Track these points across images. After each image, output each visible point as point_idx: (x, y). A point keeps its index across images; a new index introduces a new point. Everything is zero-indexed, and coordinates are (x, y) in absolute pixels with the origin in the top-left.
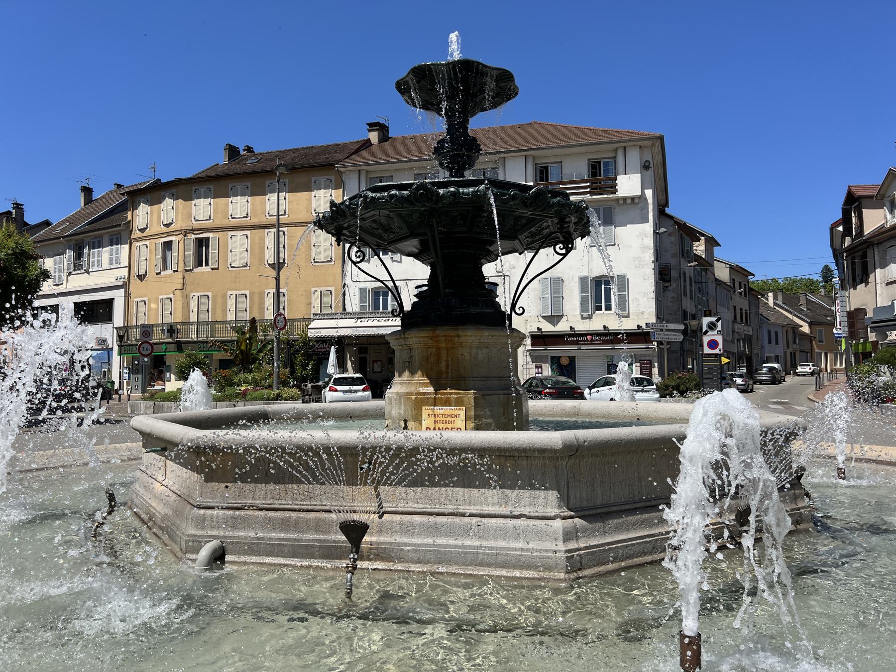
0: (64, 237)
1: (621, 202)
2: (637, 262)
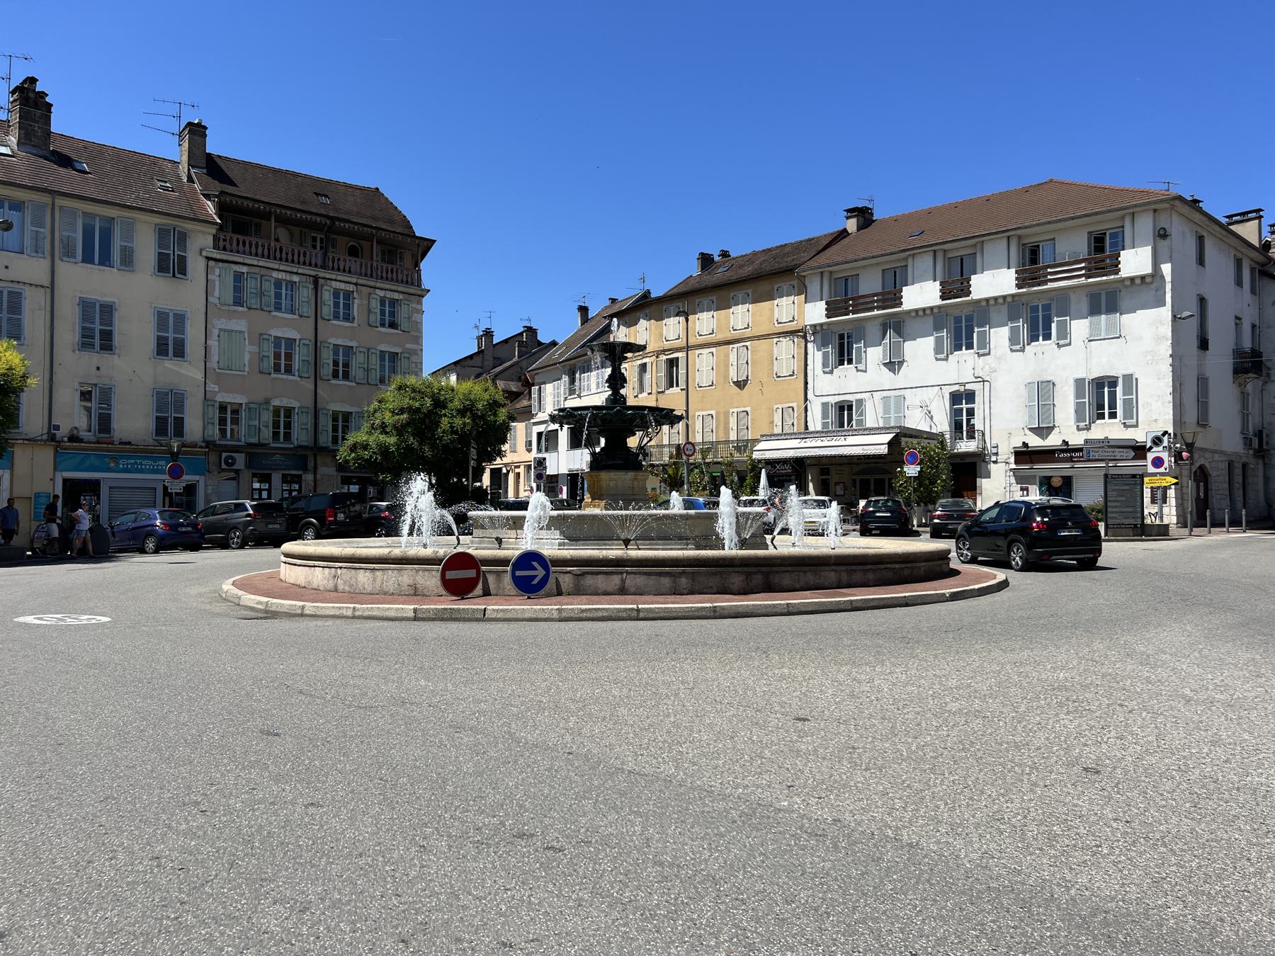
0: (559, 363)
1: (1128, 283)
2: (1149, 357)
